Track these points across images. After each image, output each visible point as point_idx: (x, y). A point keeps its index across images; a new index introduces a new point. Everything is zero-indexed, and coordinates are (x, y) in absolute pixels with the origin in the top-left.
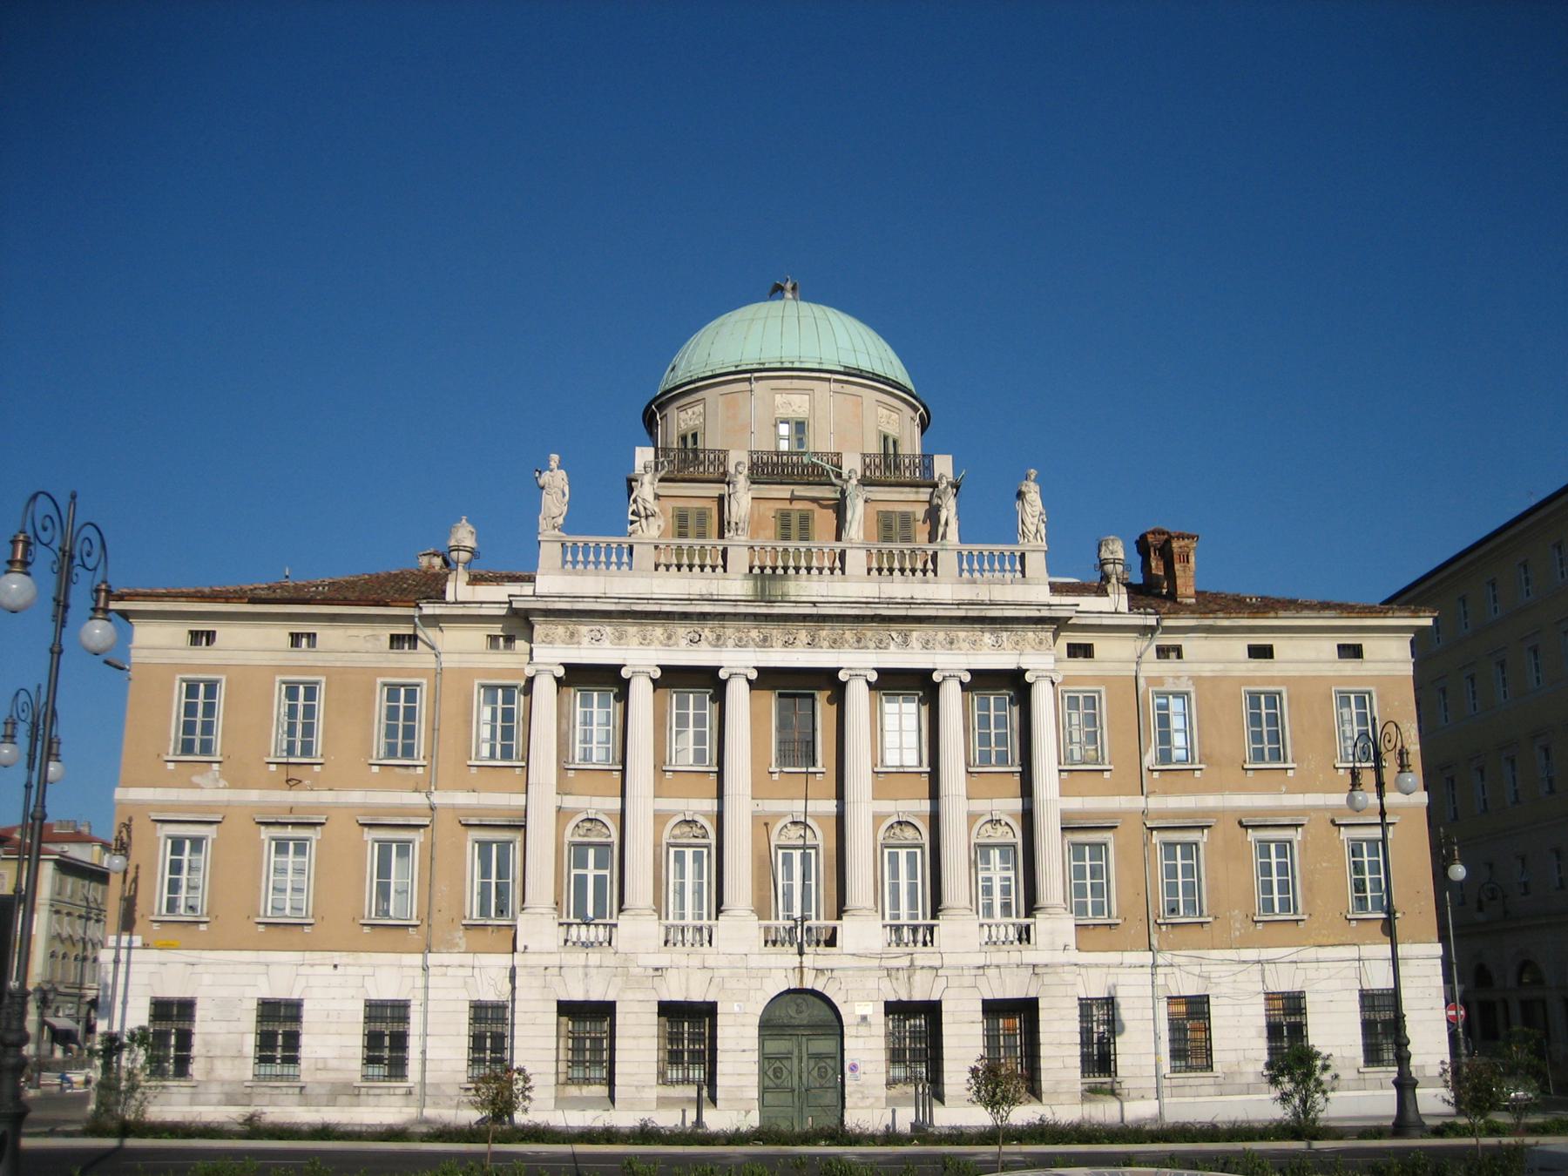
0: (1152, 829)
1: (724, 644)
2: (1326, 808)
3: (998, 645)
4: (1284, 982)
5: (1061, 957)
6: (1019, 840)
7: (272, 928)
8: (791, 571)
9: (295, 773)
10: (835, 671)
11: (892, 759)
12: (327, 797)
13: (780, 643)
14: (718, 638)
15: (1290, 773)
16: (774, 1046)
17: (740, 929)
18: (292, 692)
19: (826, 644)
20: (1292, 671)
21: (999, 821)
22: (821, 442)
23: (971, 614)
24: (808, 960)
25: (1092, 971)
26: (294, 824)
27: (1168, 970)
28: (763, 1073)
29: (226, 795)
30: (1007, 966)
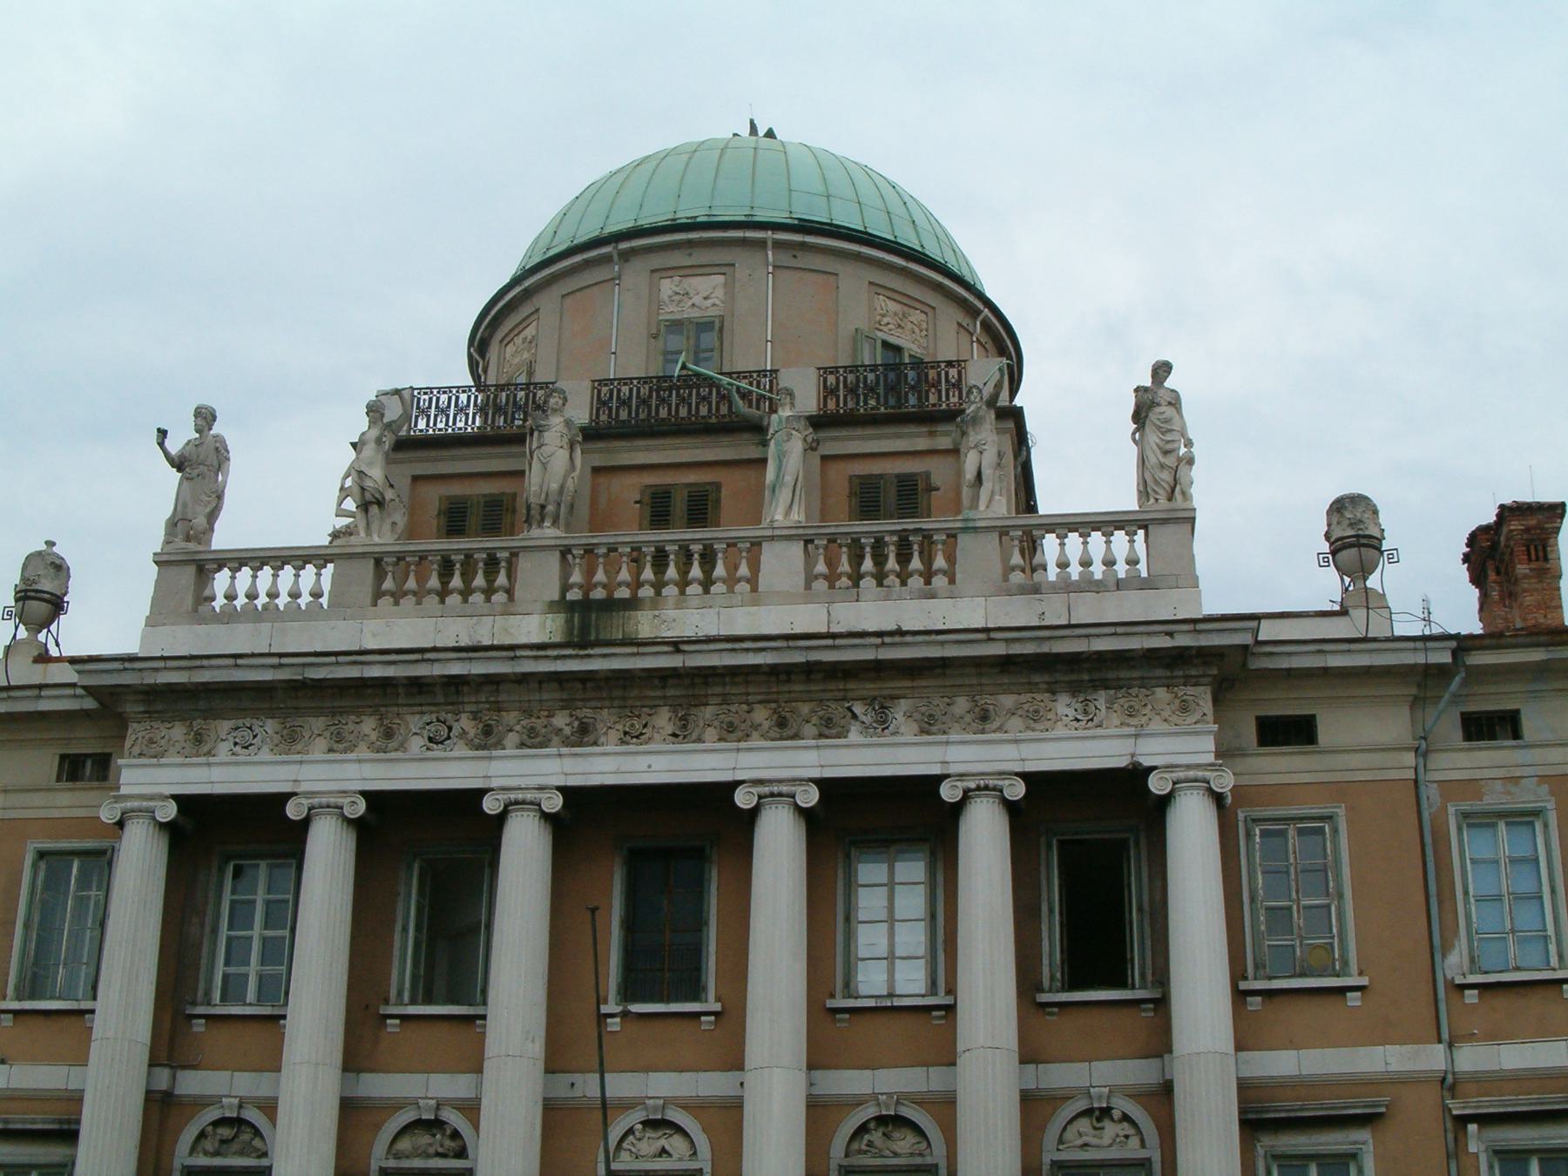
0: (1462, 1121)
1: (499, 745)
6: (1157, 1157)
8: (646, 592)
10: (1137, 775)
11: (871, 982)
13: (614, 735)
14: (487, 731)
15: (1354, 999)
19: (809, 729)
21: (1106, 1112)
22: (749, 352)
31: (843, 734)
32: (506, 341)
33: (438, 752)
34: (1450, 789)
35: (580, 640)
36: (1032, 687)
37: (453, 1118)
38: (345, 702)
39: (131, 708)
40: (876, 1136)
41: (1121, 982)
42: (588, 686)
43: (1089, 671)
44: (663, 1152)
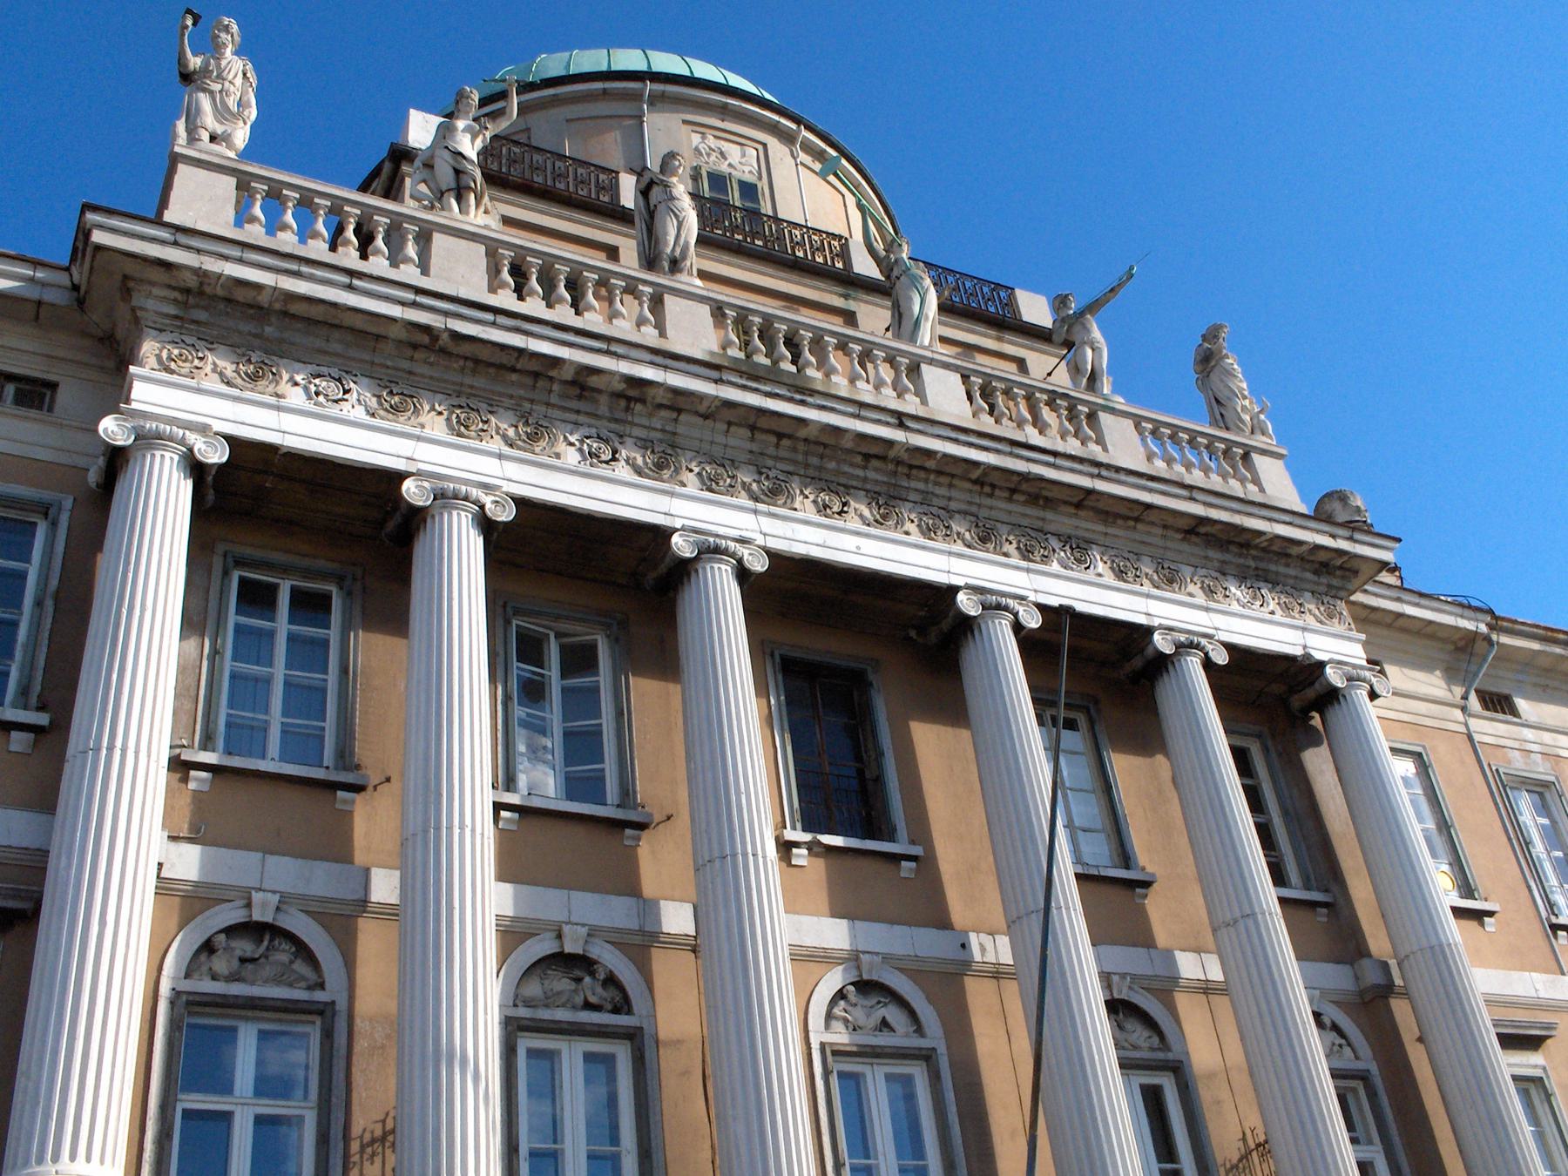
31: (1045, 559)
37: (610, 958)
38: (480, 382)
39: (154, 303)
43: (1254, 558)
44: (885, 1024)
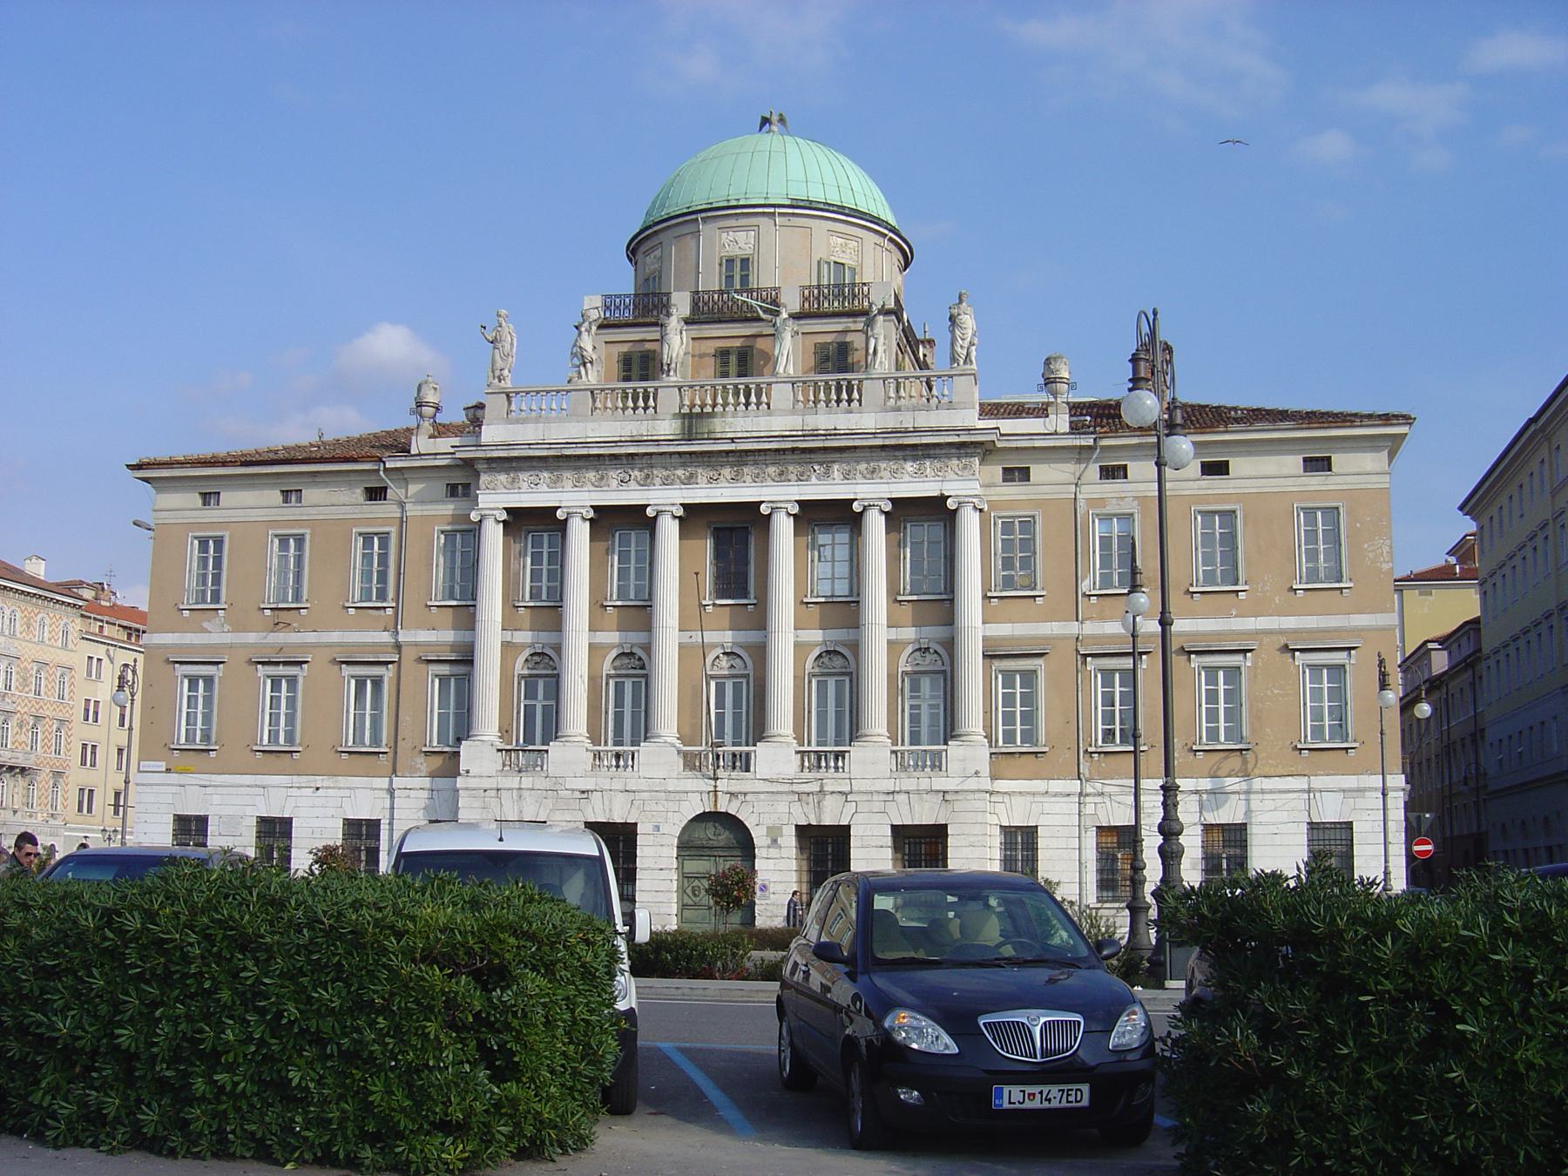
0: (1086, 656)
2: (1281, 632)
3: (920, 472)
4: (1330, 811)
5: (972, 784)
7: (273, 756)
9: (284, 616)
10: (943, 499)
12: (311, 637)
16: (693, 866)
17: (660, 759)
18: (203, 543)
20: (1250, 487)
23: (887, 442)
24: (722, 785)
25: (1016, 800)
26: (285, 663)
27: (1098, 799)
28: (682, 891)
29: (229, 638)
30: (918, 792)
32: (647, 254)
33: (625, 486)
34: (1091, 502)
35: (689, 437)
36: (896, 458)
40: (826, 660)
41: (746, 597)
42: (695, 452)
